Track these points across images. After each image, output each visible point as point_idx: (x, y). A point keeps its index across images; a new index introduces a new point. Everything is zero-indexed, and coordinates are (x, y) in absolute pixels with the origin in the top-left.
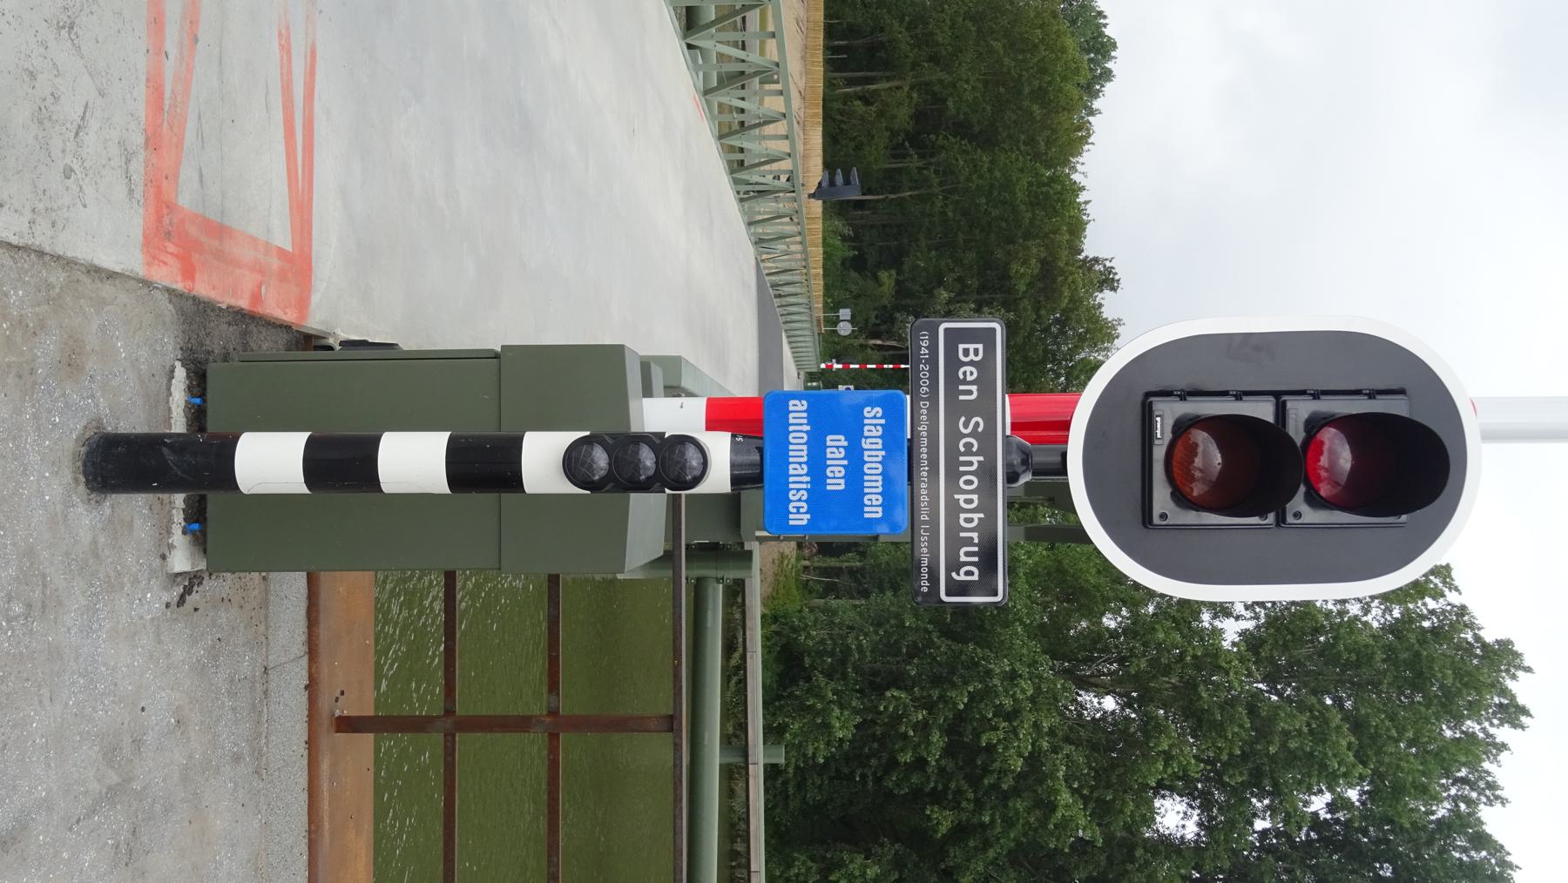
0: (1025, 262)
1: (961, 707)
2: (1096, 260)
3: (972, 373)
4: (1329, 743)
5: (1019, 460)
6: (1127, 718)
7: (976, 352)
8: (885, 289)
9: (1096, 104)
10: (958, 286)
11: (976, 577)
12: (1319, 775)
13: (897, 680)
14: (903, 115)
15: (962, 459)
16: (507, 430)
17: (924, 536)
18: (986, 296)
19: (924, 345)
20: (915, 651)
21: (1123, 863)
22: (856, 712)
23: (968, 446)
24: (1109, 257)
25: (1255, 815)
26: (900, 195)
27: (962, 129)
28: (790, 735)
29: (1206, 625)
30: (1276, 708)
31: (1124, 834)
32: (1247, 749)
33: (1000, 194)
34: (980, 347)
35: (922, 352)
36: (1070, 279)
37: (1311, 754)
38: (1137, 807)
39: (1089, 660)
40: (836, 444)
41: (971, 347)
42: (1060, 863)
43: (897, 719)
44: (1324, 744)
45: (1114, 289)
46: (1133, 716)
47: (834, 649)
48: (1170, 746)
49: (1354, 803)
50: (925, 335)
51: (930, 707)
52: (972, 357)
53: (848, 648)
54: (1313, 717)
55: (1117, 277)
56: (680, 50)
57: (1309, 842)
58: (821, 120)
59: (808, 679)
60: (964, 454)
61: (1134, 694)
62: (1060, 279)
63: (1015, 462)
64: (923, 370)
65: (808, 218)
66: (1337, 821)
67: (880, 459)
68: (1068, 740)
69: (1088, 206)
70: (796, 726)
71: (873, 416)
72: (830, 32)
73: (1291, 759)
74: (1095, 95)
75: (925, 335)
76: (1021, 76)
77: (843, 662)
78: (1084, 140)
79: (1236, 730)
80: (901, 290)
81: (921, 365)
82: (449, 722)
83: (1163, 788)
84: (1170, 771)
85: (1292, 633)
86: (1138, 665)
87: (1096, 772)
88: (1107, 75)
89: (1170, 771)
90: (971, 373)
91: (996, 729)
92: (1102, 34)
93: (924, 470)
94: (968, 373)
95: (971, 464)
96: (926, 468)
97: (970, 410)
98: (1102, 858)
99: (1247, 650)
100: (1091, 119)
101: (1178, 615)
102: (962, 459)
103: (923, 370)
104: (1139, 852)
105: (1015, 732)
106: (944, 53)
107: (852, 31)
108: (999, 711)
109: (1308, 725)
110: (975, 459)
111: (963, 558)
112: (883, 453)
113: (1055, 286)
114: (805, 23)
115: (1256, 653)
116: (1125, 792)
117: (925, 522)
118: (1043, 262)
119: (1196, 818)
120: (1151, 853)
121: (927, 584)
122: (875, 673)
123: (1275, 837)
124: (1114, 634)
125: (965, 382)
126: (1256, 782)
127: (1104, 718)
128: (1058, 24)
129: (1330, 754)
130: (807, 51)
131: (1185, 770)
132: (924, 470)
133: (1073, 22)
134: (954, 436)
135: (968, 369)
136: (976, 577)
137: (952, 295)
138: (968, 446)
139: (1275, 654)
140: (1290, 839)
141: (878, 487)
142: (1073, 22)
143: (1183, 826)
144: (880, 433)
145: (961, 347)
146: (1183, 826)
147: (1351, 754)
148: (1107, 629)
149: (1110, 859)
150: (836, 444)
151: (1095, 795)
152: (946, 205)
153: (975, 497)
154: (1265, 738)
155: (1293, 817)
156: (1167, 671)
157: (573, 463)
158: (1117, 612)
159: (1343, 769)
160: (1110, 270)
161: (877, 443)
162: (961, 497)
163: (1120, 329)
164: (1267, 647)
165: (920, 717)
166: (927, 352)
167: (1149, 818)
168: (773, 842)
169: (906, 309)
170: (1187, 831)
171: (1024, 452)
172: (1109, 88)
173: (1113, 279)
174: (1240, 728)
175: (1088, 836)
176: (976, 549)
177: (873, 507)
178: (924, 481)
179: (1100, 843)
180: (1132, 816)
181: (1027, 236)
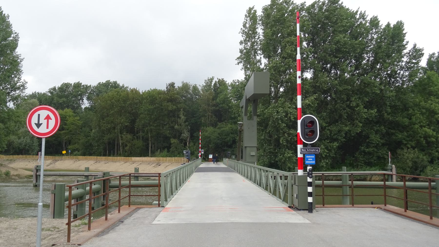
0: (168, 106)
1: (285, 125)
2: (167, 88)
8: (175, 141)
9: (121, 85)
10: (174, 123)
13: (277, 140)
14: (129, 136)
16: (307, 183)
18: (176, 116)
20: (270, 136)
22: (285, 150)
26: (150, 137)
27: (133, 122)
28: (291, 166)
33: (151, 112)
38: (307, 85)
40: (309, 159)
43: (287, 141)
45: (174, 84)
47: (270, 155)
48: (294, 77)
51: (284, 133)
53: (269, 152)
55: (171, 83)
58: (130, 157)
59: (277, 161)
62: (173, 97)
65: (159, 161)
70: (289, 165)
71: (307, 157)
72: (105, 155)
74: (119, 85)
76: (119, 106)
77: (273, 153)
80: (174, 137)
82: (323, 195)
90: (304, 150)
91: (290, 117)
97: (306, 150)
105: (291, 113)
106: (113, 126)
107: (105, 150)
108: (286, 116)
114: (105, 161)
118: (168, 102)
122: (275, 145)
130: (113, 161)
134: (308, 151)
137: (176, 124)
150: (309, 159)
151: (304, 94)
152: (153, 126)
157: (310, 178)
160: (169, 85)
163: (185, 82)
165: (287, 135)
168: (316, 170)
169: (180, 136)
172: (118, 83)
173: (172, 84)
177: (313, 157)
181: (162, 106)
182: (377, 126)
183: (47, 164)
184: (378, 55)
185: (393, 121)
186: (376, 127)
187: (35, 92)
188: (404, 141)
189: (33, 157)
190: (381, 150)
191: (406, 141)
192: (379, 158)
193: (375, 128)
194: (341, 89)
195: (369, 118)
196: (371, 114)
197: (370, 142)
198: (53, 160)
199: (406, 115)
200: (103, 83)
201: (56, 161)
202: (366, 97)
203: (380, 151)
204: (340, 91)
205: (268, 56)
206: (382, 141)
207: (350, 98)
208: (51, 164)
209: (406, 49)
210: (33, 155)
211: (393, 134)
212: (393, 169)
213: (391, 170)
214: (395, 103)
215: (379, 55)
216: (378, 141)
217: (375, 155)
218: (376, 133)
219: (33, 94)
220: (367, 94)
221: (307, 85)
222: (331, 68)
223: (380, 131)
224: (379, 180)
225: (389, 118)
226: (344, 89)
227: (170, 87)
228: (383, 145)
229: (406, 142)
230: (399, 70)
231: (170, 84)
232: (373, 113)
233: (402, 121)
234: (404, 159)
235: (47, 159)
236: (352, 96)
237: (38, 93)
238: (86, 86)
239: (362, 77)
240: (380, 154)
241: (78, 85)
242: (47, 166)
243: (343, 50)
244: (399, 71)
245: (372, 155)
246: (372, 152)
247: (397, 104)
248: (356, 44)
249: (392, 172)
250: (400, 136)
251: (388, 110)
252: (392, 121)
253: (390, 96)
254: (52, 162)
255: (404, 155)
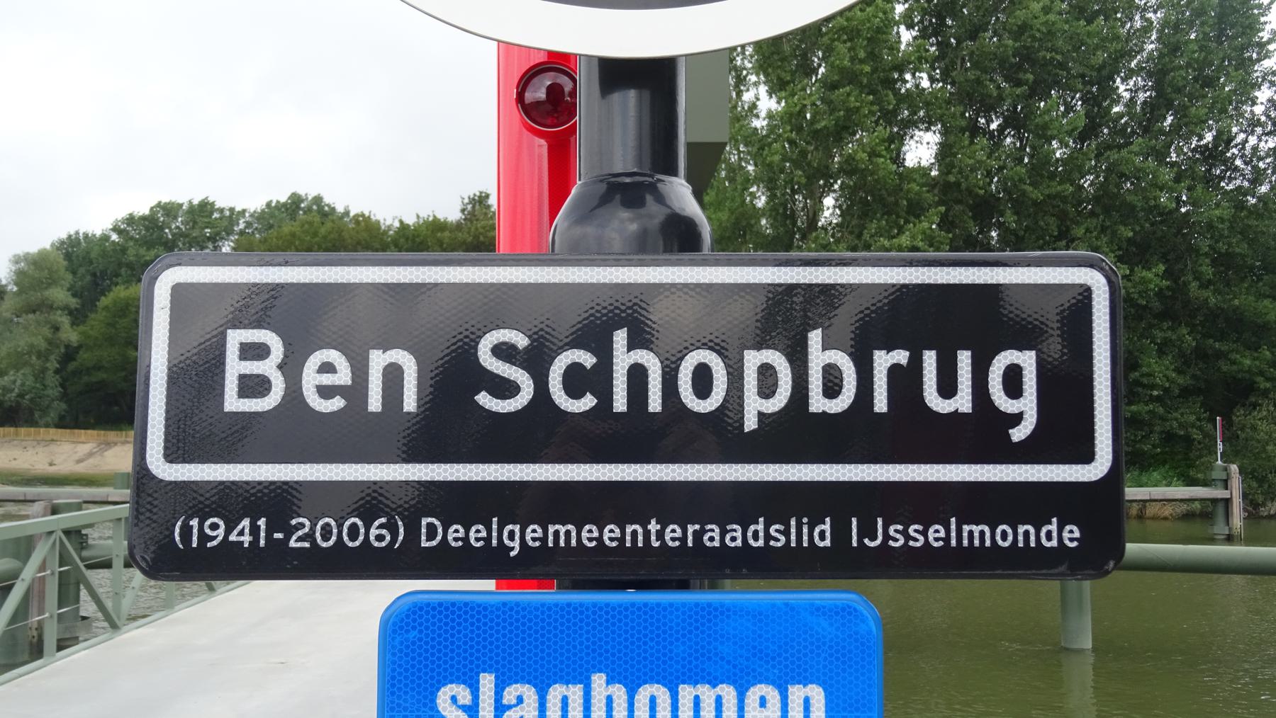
3: (327, 368)
4: (859, 27)
5: (625, 214)
6: (841, 188)
7: (254, 352)
11: (1027, 360)
12: (884, 33)
15: (620, 403)
17: (887, 537)
19: (221, 532)
21: (961, 191)
23: (576, 381)
24: (461, 200)
25: (917, 86)
29: (765, 123)
30: (831, 67)
31: (936, 191)
32: (866, 90)
34: (235, 338)
35: (246, 539)
36: (481, 230)
37: (869, 40)
39: (793, 217)
41: (235, 368)
42: (961, 243)
44: (861, 30)
46: (839, 182)
48: (864, 152)
49: (906, 9)
50: (187, 531)
52: (268, 368)
54: (838, 39)
56: (227, 594)
57: (938, 44)
60: (605, 396)
61: (821, 182)
62: (482, 238)
63: (633, 227)
64: (310, 537)
66: (921, 21)
67: (619, 692)
68: (859, 236)
69: (421, 216)
73: (873, 56)
75: (187, 531)
78: (367, 219)
79: (853, 99)
81: (293, 544)
83: (898, 159)
84: (884, 153)
85: (773, 53)
86: (800, 176)
87: (883, 214)
88: (318, 200)
89: (884, 153)
92: (285, 205)
93: (660, 535)
94: (327, 379)
95: (637, 375)
96: (654, 527)
98: (957, 208)
99: (786, 90)
100: (352, 214)
101: (757, 146)
102: (620, 403)
103: (310, 537)
104: (952, 179)
109: (845, 42)
110: (623, 359)
111: (963, 402)
112: (598, 680)
113: (487, 243)
115: (788, 83)
116: (901, 190)
117: (841, 532)
119: (921, 133)
120: (952, 168)
121: (1053, 527)
123: (935, 70)
124: (771, 198)
125: (356, 392)
126: (890, 84)
127: (840, 207)
128: (272, 239)
129: (868, 25)
131: (883, 141)
132: (660, 535)
133: (271, 227)
135: (311, 379)
136: (1027, 360)
138: (576, 381)
139: (788, 69)
140: (937, 59)
141: (719, 701)
142: (271, 227)
143: (928, 143)
144: (529, 693)
145: (233, 402)
146: (928, 143)
147: (868, 10)
148: (767, 203)
149: (959, 202)
151: (903, 214)
153: (1054, 543)
154: (857, 76)
155: (917, 60)
156: (803, 153)
158: (753, 195)
159: (881, 15)
160: (473, 201)
161: (565, 701)
162: (754, 408)
164: (783, 75)
166: (246, 523)
167: (922, 171)
170: (932, 141)
171: (605, 200)
172: (327, 200)
174: (849, 95)
175: (936, 219)
176: (930, 359)
178: (698, 535)
179: (943, 209)
180: (922, 185)
182: (1165, 325)
183: (77, 457)
184: (1169, 77)
185: (1222, 309)
186: (1162, 330)
187: (77, 233)
188: (1259, 379)
189: (49, 433)
190: (1176, 410)
191: (1267, 379)
192: (1169, 437)
193: (1159, 335)
194: (1036, 194)
195: (1136, 296)
196: (1144, 281)
197: (1145, 381)
198: (101, 444)
199: (1267, 288)
200: (278, 202)
201: (109, 445)
202: (1125, 225)
203: (1175, 414)
204: (1035, 203)
205: (777, 87)
206: (1181, 381)
207: (1068, 229)
208: (90, 455)
209: (1269, 57)
210: (47, 426)
211: (1220, 355)
212: (1234, 480)
213: (1226, 484)
214: (1230, 245)
215: (1174, 78)
216: (1168, 380)
217: (1158, 428)
218: (1161, 352)
219: (70, 236)
220: (1128, 213)
221: (915, 180)
222: (1001, 129)
223: (1174, 346)
224: (1171, 515)
225: (1207, 300)
226: (1049, 196)
227: (474, 207)
228: (1186, 392)
229: (1268, 385)
230: (1245, 132)
231: (474, 199)
232: (1150, 281)
233: (1255, 309)
234: (1259, 441)
235: (83, 439)
236: (1077, 223)
237: (86, 236)
238: (232, 210)
239: (1114, 155)
240: (1175, 424)
241: (205, 208)
242: (79, 461)
243: (1044, 57)
244: (1242, 136)
245: (1146, 428)
246: (1147, 417)
247: (1238, 250)
248: (1089, 34)
249: (1227, 489)
250: (1248, 362)
251: (1204, 268)
252: (1218, 308)
253: (1212, 221)
254: (95, 450)
255: (1254, 428)
